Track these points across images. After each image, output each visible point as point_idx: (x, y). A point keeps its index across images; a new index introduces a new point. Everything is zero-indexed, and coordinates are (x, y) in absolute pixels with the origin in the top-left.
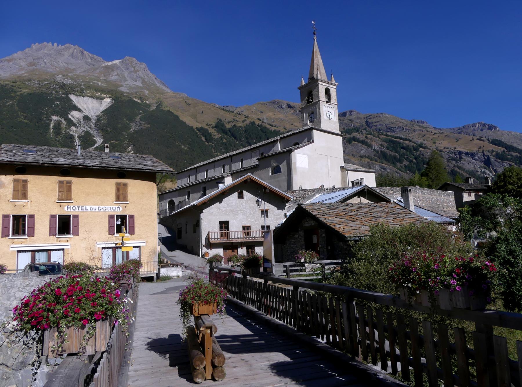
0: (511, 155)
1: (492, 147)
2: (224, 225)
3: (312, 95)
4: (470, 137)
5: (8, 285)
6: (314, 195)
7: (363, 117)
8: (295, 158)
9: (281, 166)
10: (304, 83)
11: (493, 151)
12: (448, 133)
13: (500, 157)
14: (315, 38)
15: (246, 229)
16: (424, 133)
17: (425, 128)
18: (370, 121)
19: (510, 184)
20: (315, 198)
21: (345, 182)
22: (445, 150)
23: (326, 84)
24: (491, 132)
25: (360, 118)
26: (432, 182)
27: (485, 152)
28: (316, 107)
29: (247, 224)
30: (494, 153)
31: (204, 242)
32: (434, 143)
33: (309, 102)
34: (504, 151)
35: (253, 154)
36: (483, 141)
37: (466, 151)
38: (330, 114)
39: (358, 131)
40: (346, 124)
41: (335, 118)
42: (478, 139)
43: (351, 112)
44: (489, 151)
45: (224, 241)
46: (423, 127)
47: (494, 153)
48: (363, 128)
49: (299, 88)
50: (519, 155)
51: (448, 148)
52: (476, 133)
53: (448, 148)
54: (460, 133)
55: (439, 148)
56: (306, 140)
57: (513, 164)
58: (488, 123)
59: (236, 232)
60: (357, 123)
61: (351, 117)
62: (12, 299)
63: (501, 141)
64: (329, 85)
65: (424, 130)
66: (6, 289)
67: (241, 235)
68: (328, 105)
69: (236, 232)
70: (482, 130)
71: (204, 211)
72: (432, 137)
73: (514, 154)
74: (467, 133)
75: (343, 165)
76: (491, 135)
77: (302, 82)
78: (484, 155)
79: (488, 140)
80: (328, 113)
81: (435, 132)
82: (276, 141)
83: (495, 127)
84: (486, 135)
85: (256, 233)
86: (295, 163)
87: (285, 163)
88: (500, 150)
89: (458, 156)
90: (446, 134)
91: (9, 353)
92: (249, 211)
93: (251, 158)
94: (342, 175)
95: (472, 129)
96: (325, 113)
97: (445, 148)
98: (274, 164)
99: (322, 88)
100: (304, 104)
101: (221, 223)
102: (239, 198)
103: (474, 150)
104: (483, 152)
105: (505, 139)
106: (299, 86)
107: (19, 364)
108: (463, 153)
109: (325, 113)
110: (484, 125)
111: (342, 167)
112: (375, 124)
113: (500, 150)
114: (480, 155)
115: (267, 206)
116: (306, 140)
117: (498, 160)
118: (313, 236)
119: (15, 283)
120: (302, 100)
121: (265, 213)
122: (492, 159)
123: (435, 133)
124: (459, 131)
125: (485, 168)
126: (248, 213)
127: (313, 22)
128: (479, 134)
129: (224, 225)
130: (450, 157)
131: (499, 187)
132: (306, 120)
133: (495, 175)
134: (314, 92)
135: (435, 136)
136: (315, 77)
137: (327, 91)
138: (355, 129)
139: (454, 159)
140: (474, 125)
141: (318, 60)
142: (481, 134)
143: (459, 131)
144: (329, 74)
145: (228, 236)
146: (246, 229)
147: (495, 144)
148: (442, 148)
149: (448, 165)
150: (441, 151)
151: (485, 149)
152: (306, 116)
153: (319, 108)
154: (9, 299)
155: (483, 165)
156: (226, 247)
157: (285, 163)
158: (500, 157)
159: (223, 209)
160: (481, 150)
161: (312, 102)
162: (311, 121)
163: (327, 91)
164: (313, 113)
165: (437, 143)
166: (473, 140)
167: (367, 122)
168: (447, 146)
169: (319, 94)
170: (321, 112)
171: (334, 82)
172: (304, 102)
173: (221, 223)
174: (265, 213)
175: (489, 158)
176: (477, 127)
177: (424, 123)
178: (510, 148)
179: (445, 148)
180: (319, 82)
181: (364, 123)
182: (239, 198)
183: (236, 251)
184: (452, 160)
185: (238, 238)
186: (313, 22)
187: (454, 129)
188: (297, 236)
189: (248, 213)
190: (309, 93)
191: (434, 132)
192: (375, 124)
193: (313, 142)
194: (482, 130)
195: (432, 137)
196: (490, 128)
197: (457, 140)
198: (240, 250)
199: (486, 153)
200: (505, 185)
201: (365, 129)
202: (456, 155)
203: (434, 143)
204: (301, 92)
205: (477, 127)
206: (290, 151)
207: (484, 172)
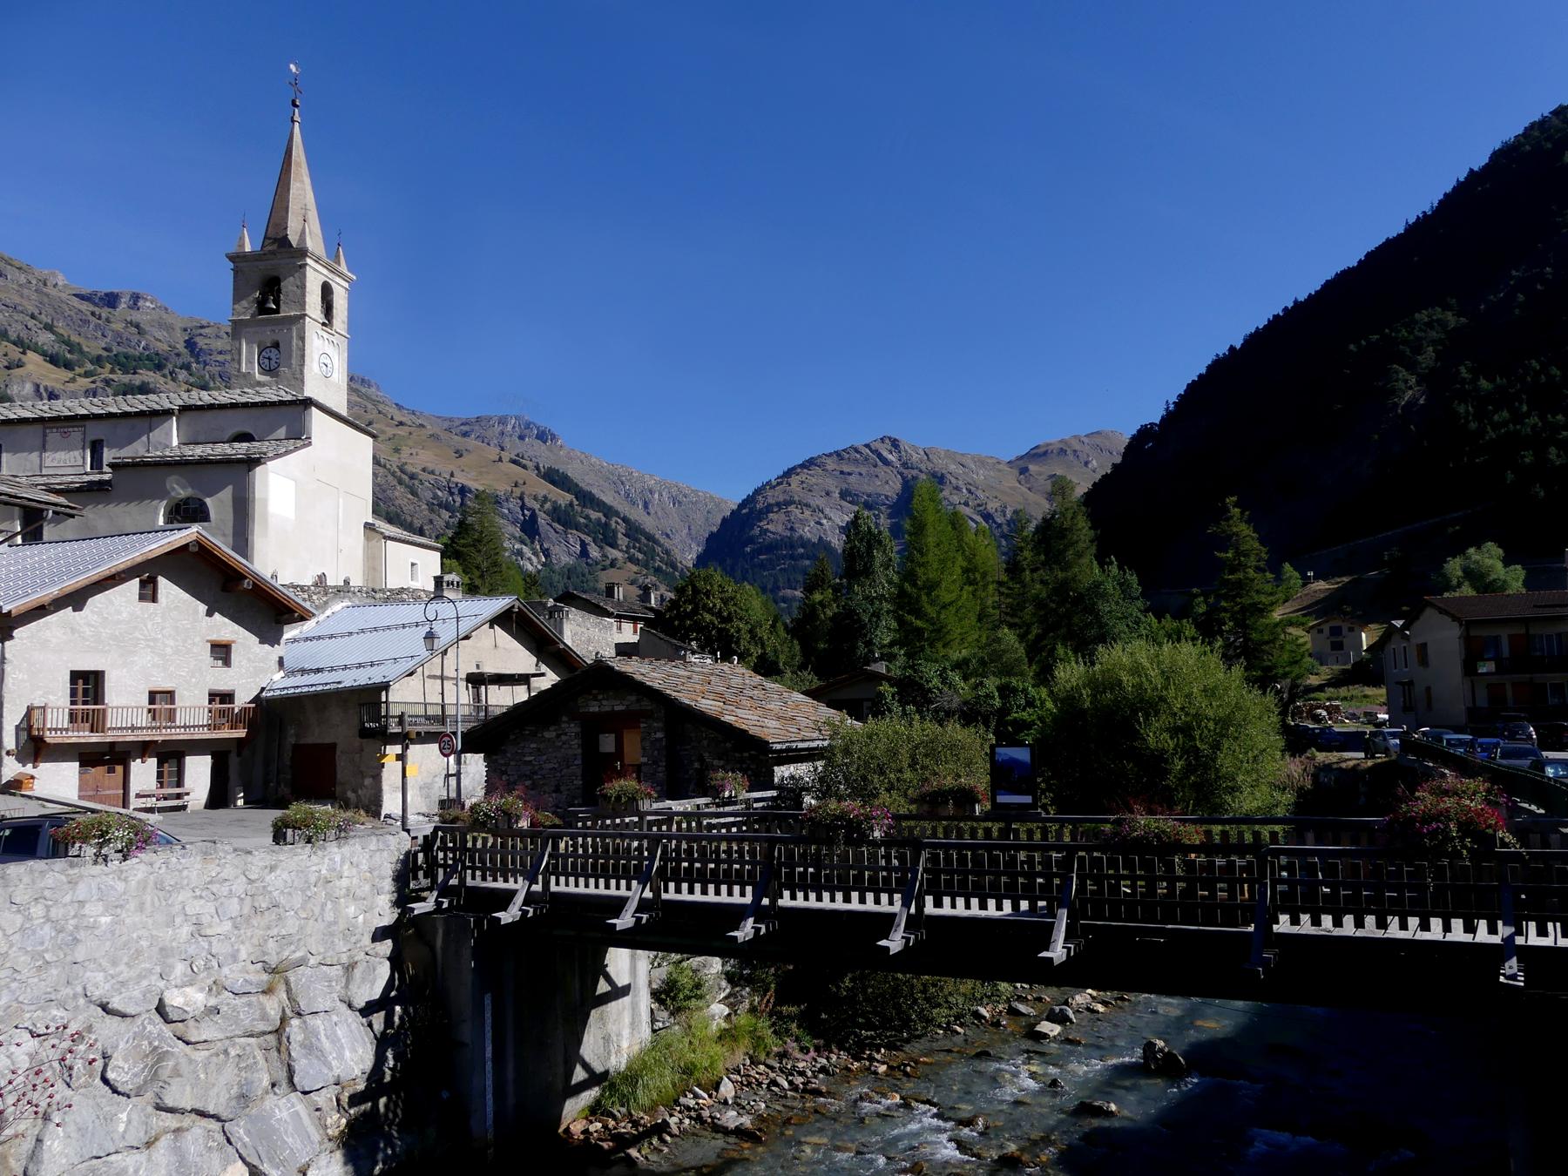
0: (587, 517)
1: (545, 488)
2: (88, 685)
3: (279, 291)
4: (493, 452)
5: (169, 881)
6: (326, 603)
7: (179, 325)
8: (266, 485)
9: (208, 501)
10: (248, 248)
11: (546, 499)
12: (437, 430)
13: (563, 518)
14: (297, 118)
15: (160, 698)
16: (369, 417)
17: (375, 403)
18: (201, 342)
19: (710, 611)
20: (328, 612)
21: (374, 569)
22: (423, 476)
23: (325, 271)
24: (543, 447)
25: (169, 328)
26: (482, 576)
27: (526, 500)
28: (290, 330)
29: (167, 686)
30: (548, 506)
31: (10, 742)
32: (397, 450)
33: (262, 309)
34: (571, 504)
35: (53, 436)
36: (524, 467)
37: (481, 488)
38: (328, 361)
39: (159, 367)
40: (118, 334)
41: (340, 376)
42: (514, 462)
43: (136, 298)
44: (535, 498)
45: (85, 736)
46: (368, 398)
47: (548, 506)
48: (179, 362)
49: (232, 258)
50: (603, 519)
51: (432, 473)
52: (507, 443)
53: (432, 473)
54: (465, 434)
55: (409, 468)
56: (282, 432)
57: (588, 539)
58: (539, 423)
59: (125, 708)
60: (160, 341)
61: (136, 316)
62: (178, 920)
63: (567, 477)
64: (331, 275)
65: (370, 406)
66: (161, 894)
67: (143, 719)
68: (326, 335)
69: (125, 708)
70: (521, 438)
71: (16, 633)
72: (391, 431)
73: (594, 515)
74: (481, 438)
75: (370, 520)
76: (545, 456)
77: (242, 239)
78: (522, 508)
79: (537, 468)
80: (325, 359)
81: (403, 419)
82: (168, 413)
83: (554, 437)
84: (531, 453)
85: (193, 715)
86: (265, 501)
87: (227, 494)
88: (564, 498)
89: (458, 499)
90: (430, 429)
91: (202, 1076)
92: (172, 643)
93: (44, 448)
94: (367, 549)
95: (497, 429)
96: (316, 357)
97: (424, 470)
98: (181, 492)
99: (315, 277)
100: (246, 310)
101: (76, 676)
102: (142, 598)
103: (502, 488)
104: (521, 498)
105: (574, 471)
106: (233, 249)
107: (234, 1103)
108: (470, 491)
109: (316, 357)
110: (528, 426)
111: (369, 527)
112: (220, 358)
113: (564, 498)
114: (514, 505)
115: (225, 628)
116: (282, 432)
117: (556, 525)
118: (601, 737)
119: (185, 873)
120: (237, 298)
121: (222, 651)
122: (543, 519)
123: (401, 423)
124: (464, 428)
125: (523, 542)
126: (169, 650)
127: (292, 67)
128: (513, 447)
129: (88, 685)
130: (435, 497)
131: (682, 617)
132: (250, 362)
133: (544, 565)
134: (288, 285)
135: (402, 431)
136: (293, 239)
137: (326, 290)
138: (149, 358)
139: (447, 507)
140: (503, 421)
141: (302, 191)
142: (521, 447)
143: (464, 428)
144: (334, 246)
145: (96, 722)
146: (160, 698)
147: (553, 483)
148: (417, 470)
149: (431, 522)
150: (412, 477)
151: (528, 490)
152: (250, 353)
153: (302, 339)
154: (171, 922)
155: (518, 532)
156: (89, 757)
157: (227, 494)
158: (563, 518)
159: (88, 631)
160: (517, 492)
161: (277, 311)
162: (270, 370)
163: (326, 290)
164: (276, 345)
165: (406, 451)
166: (500, 460)
167: (190, 344)
168: (430, 466)
169: (304, 295)
170: (307, 352)
171: (343, 268)
172: (244, 303)
173: (76, 676)
174: (222, 651)
175: (534, 516)
176: (509, 427)
177: (370, 386)
178: (586, 498)
179: (424, 470)
180: (309, 261)
181: (181, 347)
182: (142, 598)
183: (119, 769)
184: (440, 505)
185: (133, 728)
186: (292, 67)
187: (451, 420)
188: (550, 734)
189: (169, 650)
190: (268, 279)
191: (398, 417)
192: (220, 358)
193: (310, 444)
194: (521, 438)
195: (391, 431)
196: (542, 436)
197: (459, 454)
198: (136, 766)
199: (530, 502)
200: (695, 611)
201: (186, 367)
202: (452, 494)
203: (397, 450)
204: (236, 271)
205: (509, 427)
206: (252, 462)
207: (520, 553)
